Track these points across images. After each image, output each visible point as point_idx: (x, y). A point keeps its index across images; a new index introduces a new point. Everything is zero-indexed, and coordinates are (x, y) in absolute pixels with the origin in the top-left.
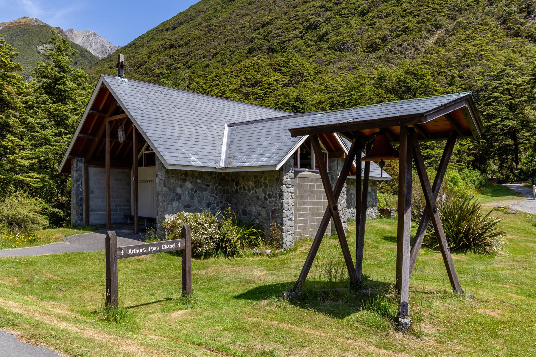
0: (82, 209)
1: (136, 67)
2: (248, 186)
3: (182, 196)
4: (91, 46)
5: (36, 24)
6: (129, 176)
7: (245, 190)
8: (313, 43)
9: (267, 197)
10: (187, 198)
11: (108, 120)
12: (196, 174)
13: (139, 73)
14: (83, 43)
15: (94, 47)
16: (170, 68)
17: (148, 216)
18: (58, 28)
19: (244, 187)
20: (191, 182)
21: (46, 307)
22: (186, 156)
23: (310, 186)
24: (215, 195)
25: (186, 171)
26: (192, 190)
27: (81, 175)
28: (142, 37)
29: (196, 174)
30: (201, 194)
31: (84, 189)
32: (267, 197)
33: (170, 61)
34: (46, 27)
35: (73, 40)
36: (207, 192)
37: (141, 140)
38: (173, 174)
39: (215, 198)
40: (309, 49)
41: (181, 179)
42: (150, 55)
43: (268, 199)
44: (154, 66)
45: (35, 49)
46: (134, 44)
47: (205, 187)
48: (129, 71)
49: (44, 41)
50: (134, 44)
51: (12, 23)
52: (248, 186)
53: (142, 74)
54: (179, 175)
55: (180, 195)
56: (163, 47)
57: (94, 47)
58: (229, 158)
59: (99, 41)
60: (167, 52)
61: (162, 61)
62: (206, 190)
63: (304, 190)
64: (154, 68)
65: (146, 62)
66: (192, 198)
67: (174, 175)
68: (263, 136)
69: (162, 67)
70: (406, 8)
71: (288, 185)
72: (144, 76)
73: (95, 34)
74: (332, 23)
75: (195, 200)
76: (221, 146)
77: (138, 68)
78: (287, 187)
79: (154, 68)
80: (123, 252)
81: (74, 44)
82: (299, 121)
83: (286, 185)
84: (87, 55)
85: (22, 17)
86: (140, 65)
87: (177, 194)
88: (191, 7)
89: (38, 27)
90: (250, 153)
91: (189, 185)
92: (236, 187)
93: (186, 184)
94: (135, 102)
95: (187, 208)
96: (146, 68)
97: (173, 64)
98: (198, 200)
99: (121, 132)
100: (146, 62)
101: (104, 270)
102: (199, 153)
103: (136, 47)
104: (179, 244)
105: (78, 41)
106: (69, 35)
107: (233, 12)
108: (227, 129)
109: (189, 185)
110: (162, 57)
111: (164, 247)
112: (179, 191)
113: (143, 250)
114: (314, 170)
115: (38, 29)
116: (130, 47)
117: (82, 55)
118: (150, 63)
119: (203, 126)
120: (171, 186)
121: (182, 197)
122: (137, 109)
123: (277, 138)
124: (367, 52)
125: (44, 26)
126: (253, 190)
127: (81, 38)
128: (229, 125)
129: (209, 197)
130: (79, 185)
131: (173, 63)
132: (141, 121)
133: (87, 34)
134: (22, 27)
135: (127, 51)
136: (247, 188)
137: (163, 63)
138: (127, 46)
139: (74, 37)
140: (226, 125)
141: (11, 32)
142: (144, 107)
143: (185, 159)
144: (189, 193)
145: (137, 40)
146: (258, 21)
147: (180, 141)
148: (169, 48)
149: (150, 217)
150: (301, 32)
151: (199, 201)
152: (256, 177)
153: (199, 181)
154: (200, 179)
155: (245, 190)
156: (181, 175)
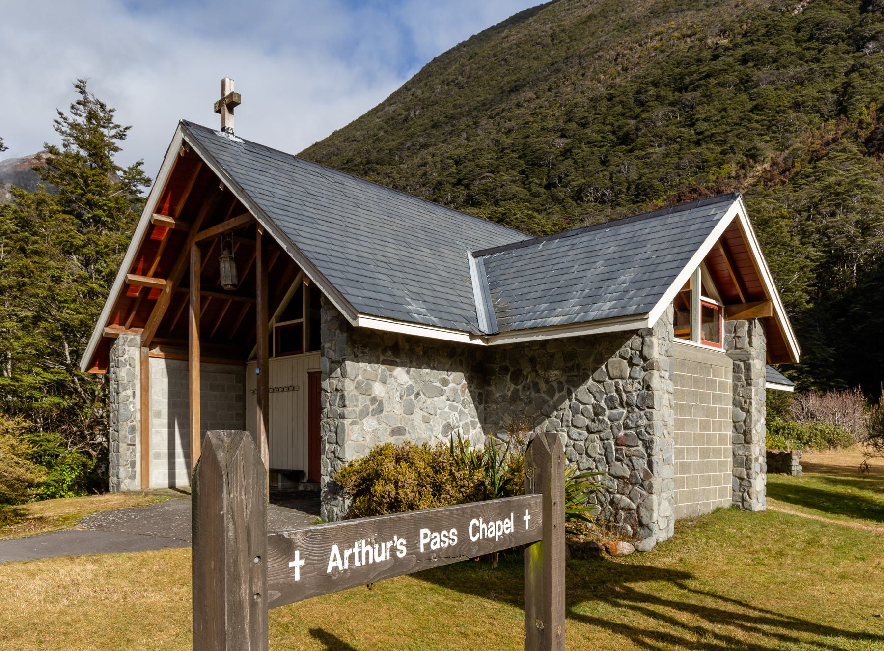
0: (133, 452)
2: (547, 381)
3: (385, 403)
6: (242, 380)
7: (538, 391)
8: (542, 190)
9: (603, 404)
10: (398, 410)
11: (197, 239)
17: (285, 468)
19: (536, 385)
22: (400, 300)
24: (460, 406)
26: (410, 389)
27: (133, 374)
30: (429, 401)
31: (138, 406)
32: (603, 404)
36: (444, 398)
37: (281, 267)
39: (461, 413)
40: (537, 200)
43: (607, 412)
47: (438, 384)
52: (547, 381)
55: (381, 403)
58: (498, 313)
62: (441, 393)
63: (683, 391)
67: (367, 351)
68: (579, 262)
70: (703, 128)
74: (576, 157)
75: (418, 416)
76: (470, 290)
80: (297, 563)
82: (669, 221)
87: (374, 400)
88: (334, 134)
90: (557, 299)
92: (512, 387)
94: (264, 182)
98: (424, 417)
99: (227, 265)
101: (190, 527)
102: (426, 298)
104: (527, 518)
107: (406, 140)
108: (472, 261)
111: (476, 529)
113: (393, 550)
119: (422, 249)
120: (360, 378)
122: (269, 194)
123: (622, 260)
124: (638, 202)
126: (561, 390)
128: (476, 255)
129: (447, 410)
130: (128, 397)
132: (280, 217)
136: (543, 386)
140: (469, 255)
142: (286, 194)
143: (398, 307)
146: (448, 155)
147: (379, 269)
149: (290, 468)
150: (523, 172)
151: (425, 420)
152: (569, 356)
155: (538, 391)
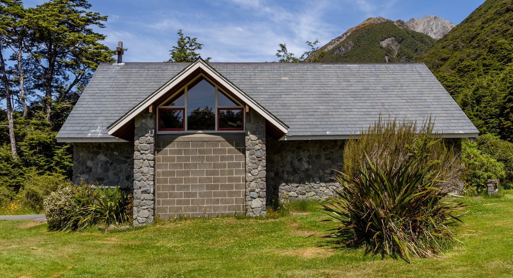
1: (468, 42)
3: (93, 169)
4: (432, 30)
5: (379, 22)
10: (99, 171)
12: (113, 146)
13: (471, 47)
14: (424, 30)
15: (435, 31)
16: (505, 34)
18: (399, 21)
20: (106, 155)
21: (372, 251)
23: (201, 152)
25: (100, 144)
26: (106, 162)
28: (479, 9)
29: (113, 146)
30: (118, 166)
33: (505, 27)
34: (389, 23)
35: (414, 28)
38: (83, 147)
41: (92, 152)
42: (484, 25)
44: (487, 36)
45: (378, 45)
46: (471, 18)
48: (461, 47)
49: (386, 37)
50: (471, 18)
51: (359, 27)
53: (475, 48)
54: (91, 148)
56: (497, 14)
57: (435, 31)
59: (440, 23)
60: (502, 18)
61: (495, 29)
64: (487, 38)
65: (479, 34)
66: (107, 170)
67: (84, 149)
69: (496, 36)
71: (142, 152)
72: (476, 49)
73: (435, 18)
75: (111, 173)
77: (470, 42)
78: (142, 154)
79: (487, 38)
81: (414, 32)
83: (139, 151)
84: (427, 40)
85: (367, 19)
86: (473, 39)
87: (87, 167)
89: (380, 24)
91: (102, 157)
93: (98, 157)
95: (100, 180)
96: (478, 40)
97: (509, 30)
100: (479, 34)
103: (473, 21)
105: (419, 29)
106: (410, 25)
109: (102, 157)
110: (496, 25)
112: (89, 163)
114: (216, 131)
115: (380, 27)
116: (466, 22)
117: (423, 42)
118: (483, 33)
120: (80, 159)
121: (94, 170)
125: (386, 23)
127: (422, 25)
131: (509, 28)
133: (428, 19)
134: (367, 28)
135: (463, 27)
137: (497, 31)
138: (463, 22)
139: (416, 26)
141: (357, 35)
144: (102, 165)
145: (473, 13)
148: (504, 13)
153: (115, 153)
154: (117, 151)
156: (93, 148)
